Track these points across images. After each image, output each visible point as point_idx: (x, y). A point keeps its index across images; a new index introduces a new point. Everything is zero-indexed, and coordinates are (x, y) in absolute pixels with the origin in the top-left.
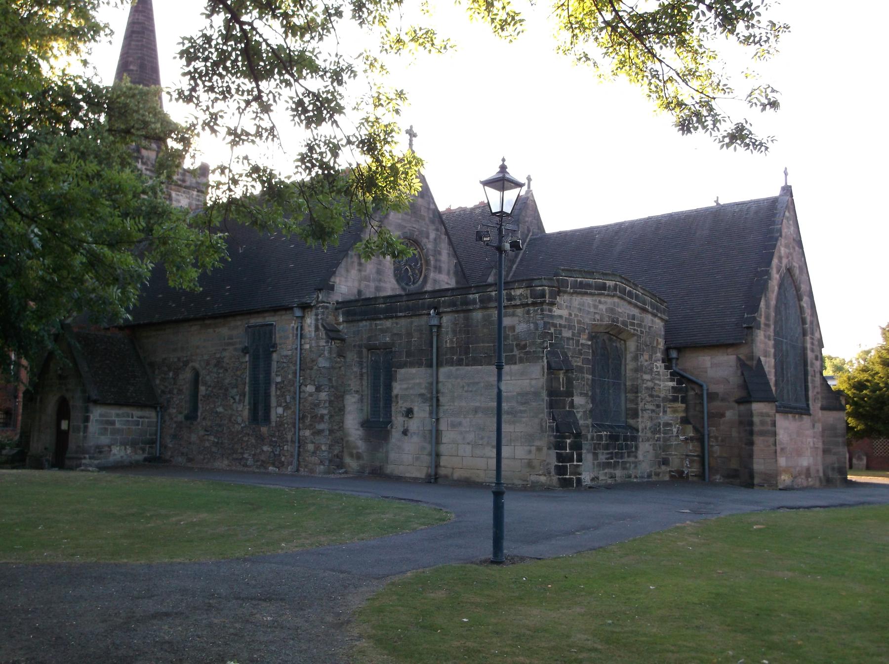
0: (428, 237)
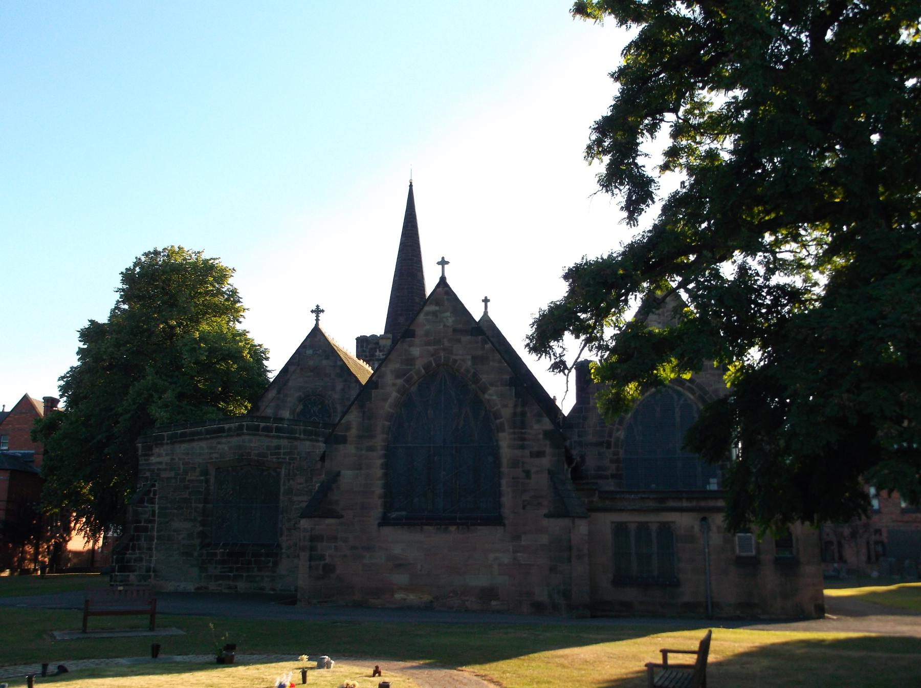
0: (333, 389)
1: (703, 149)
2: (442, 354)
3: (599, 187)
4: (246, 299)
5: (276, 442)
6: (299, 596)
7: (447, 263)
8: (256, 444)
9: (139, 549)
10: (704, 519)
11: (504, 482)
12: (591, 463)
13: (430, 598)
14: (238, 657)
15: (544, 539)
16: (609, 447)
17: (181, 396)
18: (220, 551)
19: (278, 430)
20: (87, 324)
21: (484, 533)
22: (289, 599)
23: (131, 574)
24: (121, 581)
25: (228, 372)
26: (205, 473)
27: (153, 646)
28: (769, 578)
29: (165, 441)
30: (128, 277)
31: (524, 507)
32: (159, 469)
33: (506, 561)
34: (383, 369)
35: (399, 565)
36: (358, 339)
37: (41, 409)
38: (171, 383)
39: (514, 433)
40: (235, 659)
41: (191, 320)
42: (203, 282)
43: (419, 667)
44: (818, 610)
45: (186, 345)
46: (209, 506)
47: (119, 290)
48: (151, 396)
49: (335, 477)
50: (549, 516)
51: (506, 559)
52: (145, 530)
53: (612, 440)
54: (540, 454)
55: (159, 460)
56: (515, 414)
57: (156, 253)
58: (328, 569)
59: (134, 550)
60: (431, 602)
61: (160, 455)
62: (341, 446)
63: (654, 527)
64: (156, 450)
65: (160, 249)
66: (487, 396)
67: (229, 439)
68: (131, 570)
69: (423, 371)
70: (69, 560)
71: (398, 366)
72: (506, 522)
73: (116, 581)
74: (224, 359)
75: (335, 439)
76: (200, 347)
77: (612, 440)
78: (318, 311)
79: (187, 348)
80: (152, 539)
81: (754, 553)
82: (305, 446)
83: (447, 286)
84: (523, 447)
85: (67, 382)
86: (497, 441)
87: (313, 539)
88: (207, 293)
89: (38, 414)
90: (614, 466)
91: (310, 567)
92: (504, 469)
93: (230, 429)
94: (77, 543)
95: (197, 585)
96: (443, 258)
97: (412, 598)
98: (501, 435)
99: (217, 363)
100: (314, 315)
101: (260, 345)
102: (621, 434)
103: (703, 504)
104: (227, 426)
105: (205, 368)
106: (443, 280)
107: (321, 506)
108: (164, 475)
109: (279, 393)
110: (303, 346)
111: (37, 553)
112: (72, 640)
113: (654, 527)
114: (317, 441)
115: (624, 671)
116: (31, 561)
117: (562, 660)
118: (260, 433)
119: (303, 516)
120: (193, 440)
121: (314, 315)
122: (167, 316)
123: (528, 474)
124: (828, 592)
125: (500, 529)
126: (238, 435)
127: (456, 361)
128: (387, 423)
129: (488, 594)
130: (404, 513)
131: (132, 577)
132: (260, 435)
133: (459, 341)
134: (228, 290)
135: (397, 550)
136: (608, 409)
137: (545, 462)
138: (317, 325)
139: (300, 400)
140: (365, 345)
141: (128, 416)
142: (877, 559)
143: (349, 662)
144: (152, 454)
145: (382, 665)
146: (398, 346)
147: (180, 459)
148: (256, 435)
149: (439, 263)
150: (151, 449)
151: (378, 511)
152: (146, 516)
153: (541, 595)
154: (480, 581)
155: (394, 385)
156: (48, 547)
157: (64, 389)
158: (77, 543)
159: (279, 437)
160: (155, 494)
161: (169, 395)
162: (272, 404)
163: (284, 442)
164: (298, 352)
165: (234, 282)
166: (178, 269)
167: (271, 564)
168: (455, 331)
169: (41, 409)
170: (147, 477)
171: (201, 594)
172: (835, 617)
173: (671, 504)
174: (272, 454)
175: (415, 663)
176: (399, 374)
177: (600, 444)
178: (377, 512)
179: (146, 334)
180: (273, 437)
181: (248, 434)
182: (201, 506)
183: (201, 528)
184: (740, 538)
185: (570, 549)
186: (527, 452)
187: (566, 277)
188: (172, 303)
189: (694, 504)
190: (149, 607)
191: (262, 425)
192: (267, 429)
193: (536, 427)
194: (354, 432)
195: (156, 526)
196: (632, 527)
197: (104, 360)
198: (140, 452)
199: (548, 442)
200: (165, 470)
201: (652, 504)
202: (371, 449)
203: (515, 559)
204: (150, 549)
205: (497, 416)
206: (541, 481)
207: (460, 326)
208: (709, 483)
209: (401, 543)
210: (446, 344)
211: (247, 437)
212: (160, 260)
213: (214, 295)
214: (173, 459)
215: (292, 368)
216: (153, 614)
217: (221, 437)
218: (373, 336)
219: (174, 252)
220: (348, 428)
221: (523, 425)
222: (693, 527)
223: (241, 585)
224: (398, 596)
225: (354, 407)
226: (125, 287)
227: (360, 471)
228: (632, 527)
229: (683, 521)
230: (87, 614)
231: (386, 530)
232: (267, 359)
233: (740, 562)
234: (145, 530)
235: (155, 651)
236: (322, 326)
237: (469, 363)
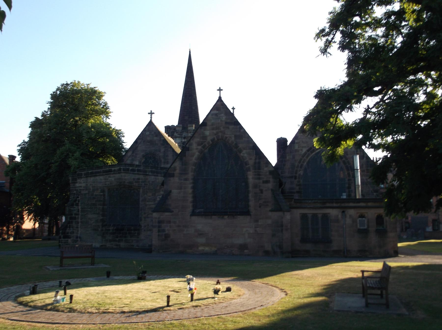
0: (160, 151)
1: (367, 35)
2: (220, 134)
4: (112, 107)
5: (137, 176)
6: (153, 249)
7: (222, 90)
8: (128, 177)
10: (343, 212)
11: (250, 195)
13: (216, 249)
14: (147, 277)
15: (269, 222)
16: (296, 178)
17: (82, 154)
19: (138, 170)
20: (34, 119)
21: (241, 218)
22: (148, 250)
23: (69, 239)
27: (107, 272)
28: (373, 239)
29: (83, 176)
30: (54, 96)
31: (260, 207)
32: (80, 190)
33: (251, 232)
34: (192, 141)
35: (201, 234)
36: (165, 127)
37: (7, 161)
38: (78, 148)
41: (85, 117)
42: (91, 99)
44: (396, 253)
45: (84, 130)
46: (105, 207)
48: (68, 154)
49: (168, 194)
50: (271, 211)
51: (251, 231)
52: (75, 218)
53: (297, 175)
54: (267, 182)
55: (80, 185)
56: (255, 163)
57: (67, 84)
58: (167, 236)
59: (70, 228)
60: (216, 251)
61: (80, 183)
62: (172, 179)
63: (320, 216)
64: (78, 181)
65: (69, 83)
66: (242, 154)
67: (114, 175)
68: (69, 237)
70: (24, 233)
71: (198, 140)
72: (252, 214)
73: (62, 243)
74: (102, 137)
75: (168, 174)
76: (92, 131)
77: (297, 175)
78: (151, 113)
79: (85, 131)
80: (78, 223)
81: (366, 227)
82: (151, 178)
83: (222, 101)
84: (259, 179)
85: (22, 147)
88: (93, 104)
89: (5, 164)
90: (298, 187)
91: (159, 235)
92: (250, 189)
93: (115, 170)
94: (28, 224)
95: (101, 244)
97: (207, 249)
98: (249, 173)
99: (99, 139)
100: (150, 115)
102: (301, 173)
103: (343, 205)
107: (162, 206)
109: (133, 153)
110: (145, 130)
111: (8, 230)
112: (58, 270)
113: (320, 216)
114: (157, 176)
115: (329, 281)
116: (5, 234)
117: (297, 277)
118: (130, 172)
119: (154, 211)
120: (97, 176)
121: (150, 115)
122: (72, 117)
123: (262, 191)
124: (399, 245)
126: (119, 173)
127: (226, 137)
128: (194, 167)
129: (243, 247)
130: (202, 210)
131: (70, 240)
132: (130, 173)
133: (228, 128)
135: (199, 227)
136: (328, 160)
137: (270, 185)
138: (151, 120)
139: (144, 156)
140: (168, 129)
141: (57, 164)
142: (406, 230)
143: (201, 278)
144: (77, 183)
145: (221, 279)
146: (199, 130)
147: (90, 185)
148: (127, 173)
150: (76, 180)
151: (190, 209)
152: (75, 212)
153: (268, 247)
154: (239, 241)
155: (197, 149)
156: (14, 227)
157: (20, 151)
158: (28, 224)
160: (79, 202)
161: (77, 154)
162: (130, 158)
163: (141, 177)
165: (105, 99)
166: (78, 92)
167: (136, 234)
168: (226, 123)
169: (7, 161)
170: (75, 193)
171: (103, 248)
172: (403, 256)
173: (328, 205)
174: (136, 182)
176: (199, 144)
177: (291, 177)
178: (190, 209)
179: (63, 124)
180: (136, 174)
183: (102, 218)
184: (360, 220)
185: (282, 226)
186: (261, 181)
187: (316, 97)
189: (339, 205)
190: (90, 255)
191: (131, 168)
192: (133, 170)
193: (266, 169)
194: (178, 171)
196: (310, 216)
197: (44, 137)
198: (71, 182)
200: (83, 190)
202: (186, 180)
203: (256, 231)
204: (77, 227)
205: (247, 164)
206: (268, 195)
207: (228, 121)
209: (201, 224)
210: (222, 129)
211: (123, 174)
213: (96, 105)
214: (87, 185)
215: (139, 141)
216: (93, 257)
218: (173, 126)
220: (175, 169)
221: (259, 168)
223: (123, 244)
224: (201, 248)
225: (177, 160)
226: (52, 101)
227: (181, 190)
228: (310, 216)
229: (334, 213)
230: (62, 258)
231: (194, 218)
232: (124, 136)
233: (360, 231)
234: (75, 218)
235: (108, 274)
236: (153, 121)
237: (233, 139)
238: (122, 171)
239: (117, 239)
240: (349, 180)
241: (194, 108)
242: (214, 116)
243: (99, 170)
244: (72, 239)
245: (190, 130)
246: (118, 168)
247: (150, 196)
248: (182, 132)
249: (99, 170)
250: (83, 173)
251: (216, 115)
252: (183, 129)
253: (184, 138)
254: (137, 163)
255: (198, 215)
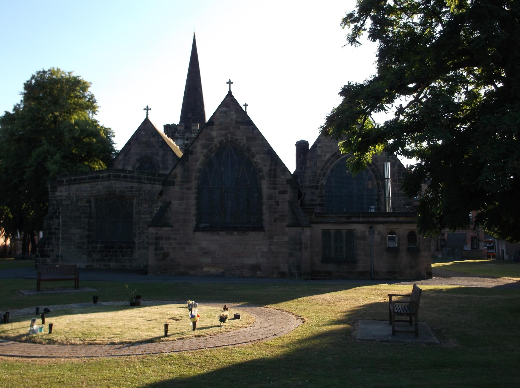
1: (402, 22)
2: (229, 136)
3: (347, 42)
4: (99, 102)
5: (130, 184)
6: (149, 270)
7: (232, 83)
9: (52, 244)
10: (371, 227)
11: (264, 207)
12: (307, 198)
13: (223, 270)
14: (142, 303)
15: (286, 239)
16: (317, 188)
17: (63, 157)
18: (99, 245)
19: (131, 177)
21: (253, 235)
22: (144, 271)
24: (42, 263)
25: (90, 144)
26: (89, 202)
27: (94, 297)
28: (404, 259)
29: (64, 183)
30: (28, 86)
31: (275, 221)
32: (61, 200)
33: (265, 250)
34: (195, 143)
35: (206, 253)
36: (165, 126)
39: (270, 181)
40: (141, 304)
42: (74, 90)
43: (238, 306)
44: (429, 275)
47: (21, 93)
49: (168, 205)
50: (288, 226)
51: (265, 249)
52: (55, 234)
54: (284, 192)
55: (61, 194)
56: (270, 170)
57: (44, 72)
58: (166, 255)
59: (49, 245)
60: (224, 272)
61: (61, 191)
62: (172, 187)
63: (344, 232)
64: (59, 189)
65: (46, 70)
66: (255, 160)
68: (48, 256)
69: (219, 145)
71: (204, 142)
72: (265, 229)
74: (88, 136)
76: (75, 129)
77: (319, 185)
78: (147, 109)
80: (59, 239)
82: (148, 187)
83: (232, 96)
84: (275, 188)
86: (260, 185)
87: (157, 238)
88: (76, 96)
91: (156, 254)
92: (264, 200)
93: (103, 177)
96: (230, 80)
97: (213, 270)
98: (263, 181)
99: (84, 138)
101: (110, 129)
102: (324, 182)
103: (371, 219)
104: (101, 175)
105: (78, 141)
106: (230, 93)
107: (160, 220)
108: (64, 203)
109: (125, 156)
110: (139, 129)
113: (344, 232)
114: (155, 184)
117: (316, 302)
119: (150, 226)
120: (81, 183)
121: (145, 111)
123: (277, 203)
124: (433, 265)
125: (262, 233)
126: (108, 180)
127: (237, 139)
128: (198, 174)
129: (255, 268)
130: (208, 225)
131: (48, 260)
132: (122, 180)
133: (239, 128)
134: (88, 95)
137: (287, 197)
139: (138, 160)
140: (168, 128)
141: (33, 168)
142: (441, 249)
144: (57, 191)
145: (228, 305)
146: (204, 131)
147: (73, 194)
149: (227, 83)
153: (284, 268)
154: (250, 261)
155: (202, 152)
159: (132, 182)
161: (58, 157)
162: (121, 163)
163: (135, 185)
164: (136, 133)
168: (237, 122)
173: (354, 219)
174: (128, 191)
175: (238, 304)
176: (204, 147)
177: (312, 187)
178: (193, 223)
181: (113, 180)
182: (87, 220)
185: (301, 244)
186: (277, 191)
187: (341, 94)
188: (56, 102)
189: (366, 219)
190: (73, 277)
191: (122, 174)
193: (282, 177)
194: (179, 179)
195: (61, 231)
196: (333, 232)
199: (289, 186)
200: (65, 200)
201: (344, 220)
202: (189, 189)
203: (270, 249)
204: (58, 245)
205: (260, 171)
206: (285, 207)
207: (240, 120)
208: (370, 209)
209: (206, 241)
211: (113, 182)
212: (47, 76)
213: (80, 98)
214: (69, 194)
215: (133, 142)
216: (77, 280)
217: (98, 181)
218: (174, 125)
219: (54, 72)
220: (175, 177)
221: (275, 176)
222: (365, 232)
223: (113, 264)
224: (205, 269)
227: (183, 202)
228: (333, 232)
229: (360, 228)
230: (39, 281)
231: (198, 234)
232: (114, 136)
233: (390, 250)
234: (55, 234)
235: (95, 300)
236: (150, 118)
237: (245, 141)
238: (112, 178)
239: (106, 258)
240: (378, 191)
241: (199, 104)
242: (222, 114)
243: (84, 177)
244: (51, 258)
245: (194, 130)
246: (107, 174)
247: (145, 208)
248: (184, 132)
249: (84, 177)
250: (64, 179)
251: (225, 112)
252: (185, 129)
253: (187, 139)
254: (130, 168)
255: (203, 231)
